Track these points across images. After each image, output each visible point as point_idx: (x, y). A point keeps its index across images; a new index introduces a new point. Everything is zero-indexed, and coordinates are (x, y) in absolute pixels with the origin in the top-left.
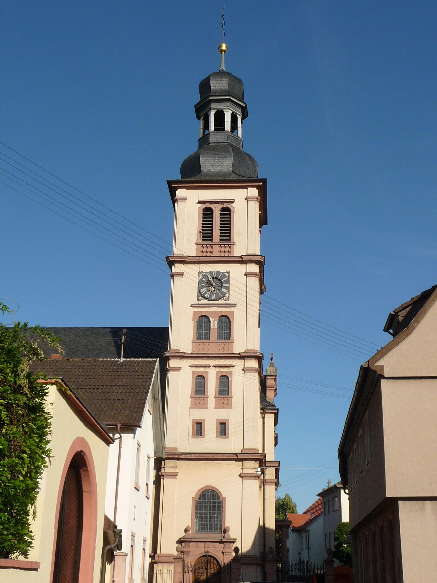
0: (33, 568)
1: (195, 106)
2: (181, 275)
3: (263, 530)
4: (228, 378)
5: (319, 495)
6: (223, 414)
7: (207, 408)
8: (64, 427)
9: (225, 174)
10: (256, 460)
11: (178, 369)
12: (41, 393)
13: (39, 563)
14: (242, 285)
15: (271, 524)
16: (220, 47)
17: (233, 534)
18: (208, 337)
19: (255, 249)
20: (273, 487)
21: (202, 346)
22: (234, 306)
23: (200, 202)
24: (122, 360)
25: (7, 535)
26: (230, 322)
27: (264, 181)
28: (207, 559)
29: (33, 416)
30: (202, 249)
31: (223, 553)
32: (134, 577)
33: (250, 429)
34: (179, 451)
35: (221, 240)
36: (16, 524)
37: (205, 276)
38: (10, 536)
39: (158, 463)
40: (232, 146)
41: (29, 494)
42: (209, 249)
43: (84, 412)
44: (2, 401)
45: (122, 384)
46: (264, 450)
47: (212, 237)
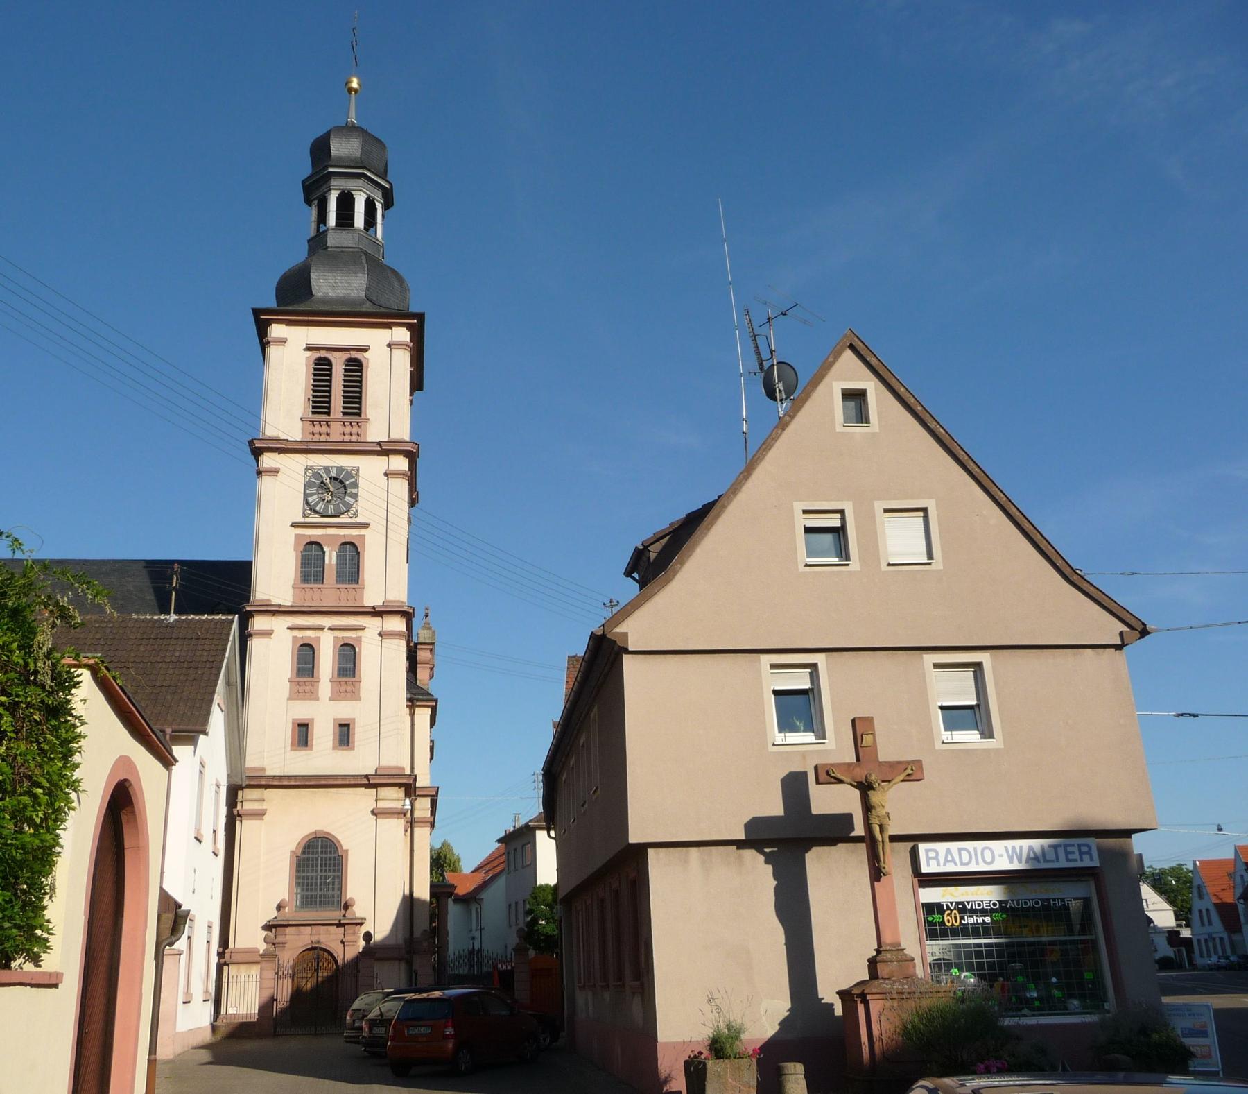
0: (51, 983)
1: (303, 182)
2: (275, 472)
3: (409, 902)
4: (353, 647)
5: (499, 841)
6: (345, 710)
7: (317, 699)
8: (101, 741)
9: (353, 302)
10: (400, 785)
11: (268, 634)
12: (66, 682)
13: (62, 974)
14: (379, 492)
15: (423, 892)
16: (348, 83)
17: (359, 911)
18: (319, 577)
19: (402, 431)
20: (428, 829)
21: (309, 593)
22: (365, 526)
23: (309, 348)
24: (173, 617)
25: (10, 928)
26: (358, 553)
27: (421, 317)
28: (317, 953)
29: (53, 722)
30: (311, 429)
31: (342, 942)
32: (193, 990)
33: (388, 730)
34: (268, 773)
35: (344, 414)
36: (23, 909)
37: (317, 475)
38: (14, 931)
39: (233, 792)
40: (366, 254)
41: (44, 857)
42: (324, 429)
43: (131, 712)
44: (3, 699)
45: (174, 659)
46: (412, 768)
47: (329, 408)
